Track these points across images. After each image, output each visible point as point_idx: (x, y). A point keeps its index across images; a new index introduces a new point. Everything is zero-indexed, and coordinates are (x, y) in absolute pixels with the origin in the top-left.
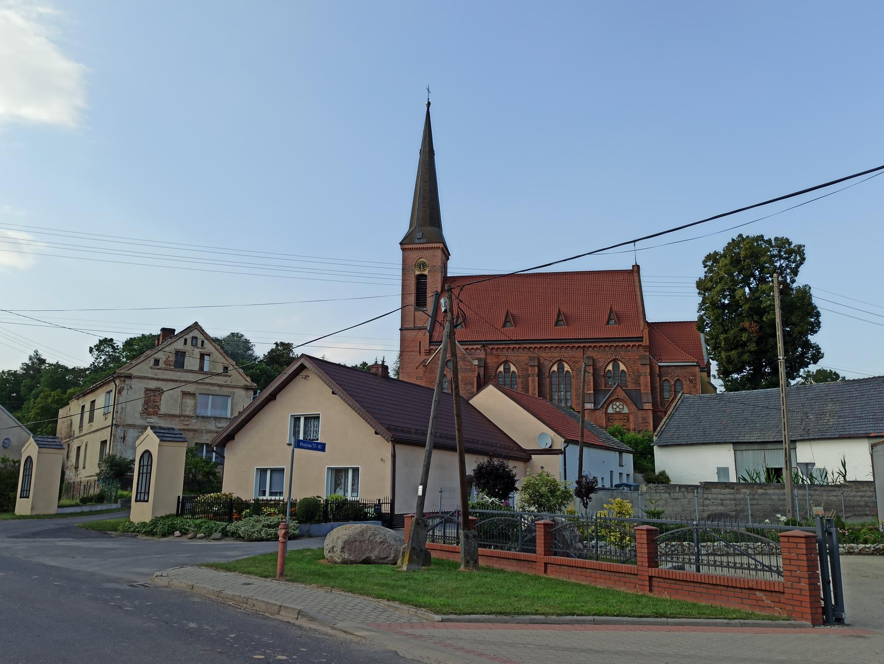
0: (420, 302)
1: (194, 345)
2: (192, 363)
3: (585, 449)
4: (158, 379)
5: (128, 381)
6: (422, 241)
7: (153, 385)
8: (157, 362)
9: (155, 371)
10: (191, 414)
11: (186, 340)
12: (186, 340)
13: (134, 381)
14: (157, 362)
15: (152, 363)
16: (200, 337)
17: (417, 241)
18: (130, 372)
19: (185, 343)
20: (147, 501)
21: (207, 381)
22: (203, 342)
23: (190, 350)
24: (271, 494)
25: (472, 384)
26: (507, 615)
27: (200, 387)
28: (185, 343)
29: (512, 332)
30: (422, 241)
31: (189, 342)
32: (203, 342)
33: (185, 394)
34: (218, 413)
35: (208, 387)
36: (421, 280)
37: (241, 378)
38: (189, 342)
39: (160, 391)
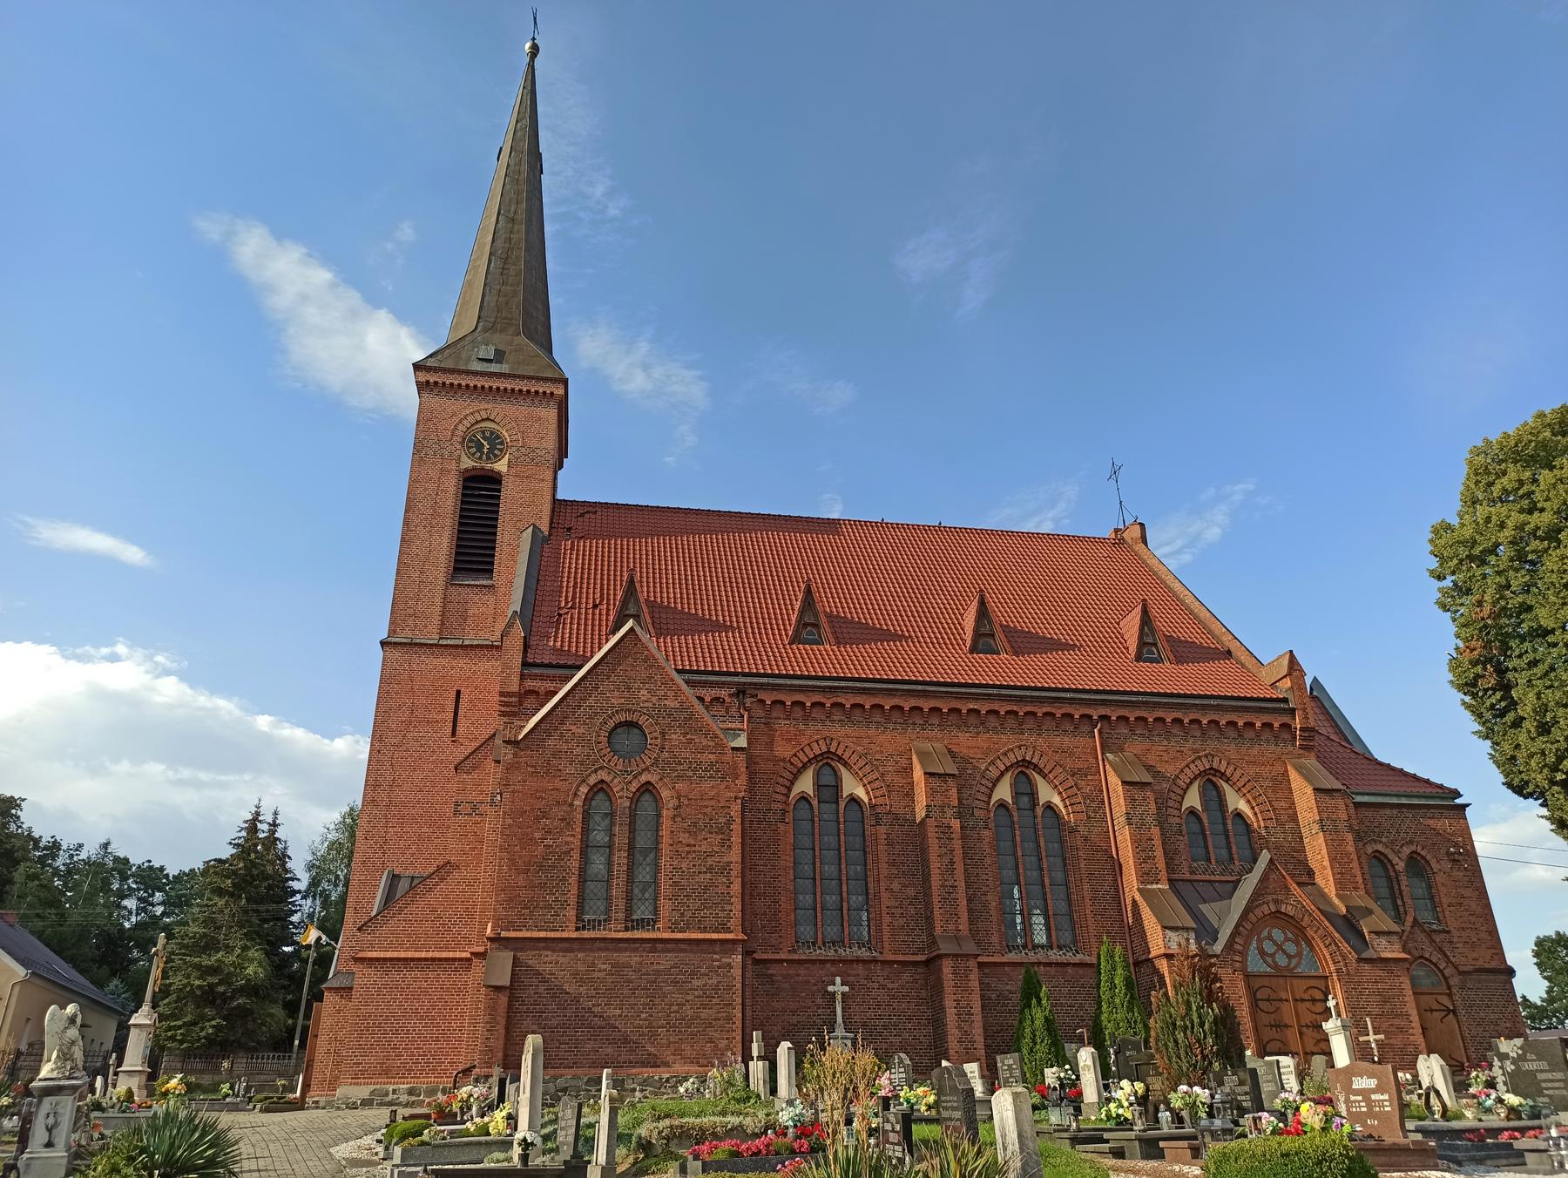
0: (474, 552)
6: (494, 368)
17: (477, 366)
25: (724, 830)
30: (494, 368)
36: (480, 492)
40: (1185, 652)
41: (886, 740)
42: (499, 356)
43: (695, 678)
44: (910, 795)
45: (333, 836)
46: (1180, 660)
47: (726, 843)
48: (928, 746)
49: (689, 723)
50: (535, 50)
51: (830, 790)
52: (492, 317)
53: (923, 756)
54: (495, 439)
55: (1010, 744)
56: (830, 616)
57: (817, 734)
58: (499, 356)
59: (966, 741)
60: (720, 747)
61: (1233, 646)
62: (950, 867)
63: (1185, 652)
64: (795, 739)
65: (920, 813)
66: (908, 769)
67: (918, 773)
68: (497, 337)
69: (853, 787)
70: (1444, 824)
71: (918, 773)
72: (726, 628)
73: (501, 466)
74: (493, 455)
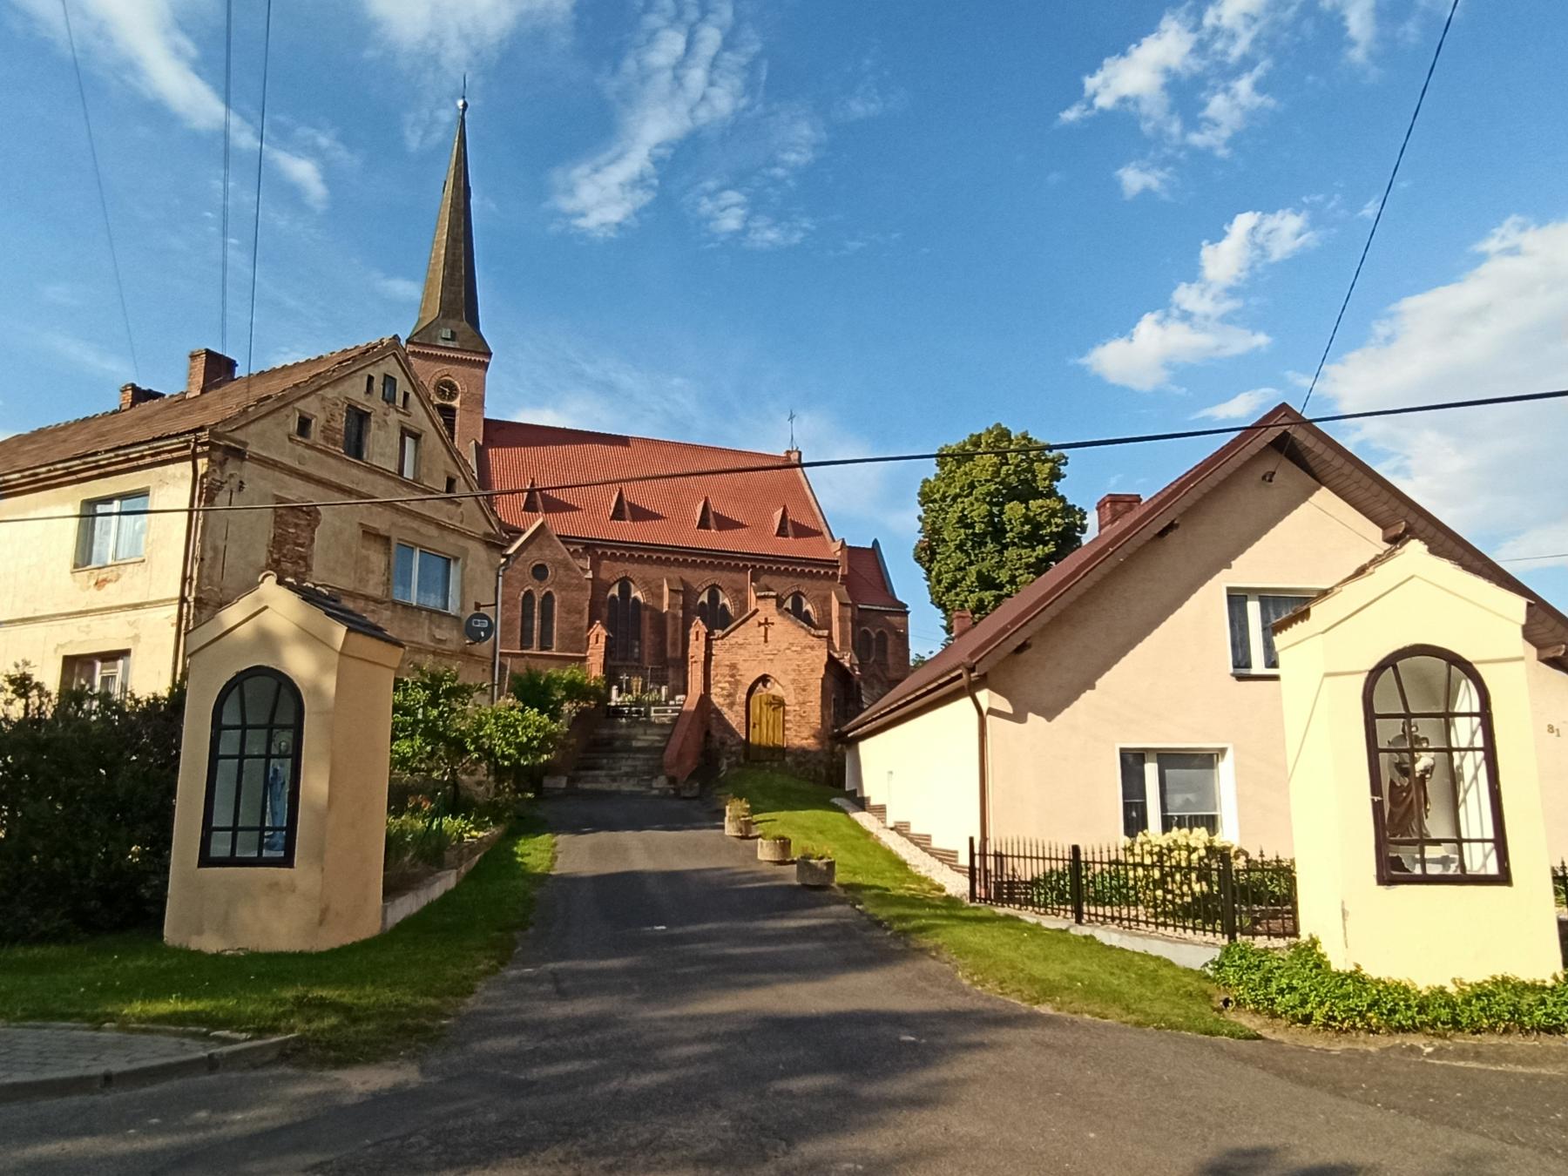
1: (389, 399)
2: (381, 444)
3: (265, 732)
4: (307, 478)
5: (231, 467)
6: (451, 344)
7: (298, 492)
8: (304, 424)
9: (300, 449)
10: (378, 592)
11: (370, 379)
12: (370, 379)
13: (249, 470)
14: (304, 424)
15: (293, 426)
16: (402, 385)
17: (441, 343)
18: (239, 435)
19: (369, 389)
20: (1503, 878)
21: (414, 506)
22: (406, 395)
23: (380, 411)
24: (1167, 825)
25: (581, 612)
26: (748, 986)
27: (401, 520)
28: (369, 389)
29: (628, 531)
30: (451, 344)
31: (378, 385)
32: (406, 395)
33: (369, 534)
34: (434, 602)
35: (415, 524)
37: (479, 514)
38: (378, 385)
39: (310, 514)
40: (802, 531)
41: (651, 571)
42: (453, 337)
43: (565, 539)
44: (661, 597)
45: (1451, 989)
46: (796, 536)
47: (581, 618)
48: (671, 576)
49: (567, 567)
50: (465, 105)
51: (625, 591)
52: (447, 310)
53: (669, 581)
54: (452, 387)
55: (710, 577)
56: (630, 504)
57: (621, 569)
58: (453, 337)
59: (688, 574)
60: (580, 578)
61: (825, 530)
62: (676, 630)
63: (802, 531)
64: (611, 571)
65: (665, 609)
66: (661, 586)
67: (666, 589)
68: (452, 322)
69: (637, 594)
70: (895, 620)
71: (666, 589)
72: (576, 509)
73: (456, 403)
74: (452, 397)
